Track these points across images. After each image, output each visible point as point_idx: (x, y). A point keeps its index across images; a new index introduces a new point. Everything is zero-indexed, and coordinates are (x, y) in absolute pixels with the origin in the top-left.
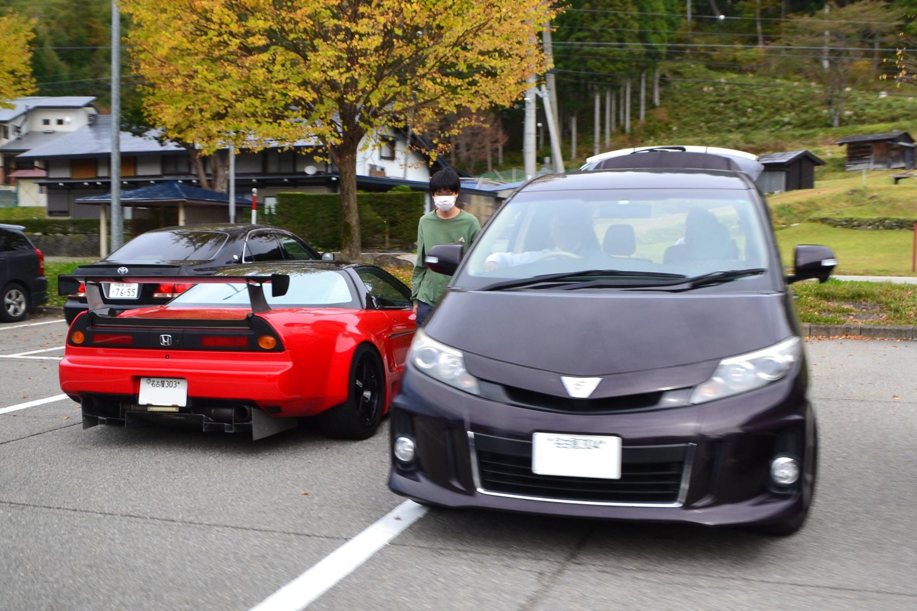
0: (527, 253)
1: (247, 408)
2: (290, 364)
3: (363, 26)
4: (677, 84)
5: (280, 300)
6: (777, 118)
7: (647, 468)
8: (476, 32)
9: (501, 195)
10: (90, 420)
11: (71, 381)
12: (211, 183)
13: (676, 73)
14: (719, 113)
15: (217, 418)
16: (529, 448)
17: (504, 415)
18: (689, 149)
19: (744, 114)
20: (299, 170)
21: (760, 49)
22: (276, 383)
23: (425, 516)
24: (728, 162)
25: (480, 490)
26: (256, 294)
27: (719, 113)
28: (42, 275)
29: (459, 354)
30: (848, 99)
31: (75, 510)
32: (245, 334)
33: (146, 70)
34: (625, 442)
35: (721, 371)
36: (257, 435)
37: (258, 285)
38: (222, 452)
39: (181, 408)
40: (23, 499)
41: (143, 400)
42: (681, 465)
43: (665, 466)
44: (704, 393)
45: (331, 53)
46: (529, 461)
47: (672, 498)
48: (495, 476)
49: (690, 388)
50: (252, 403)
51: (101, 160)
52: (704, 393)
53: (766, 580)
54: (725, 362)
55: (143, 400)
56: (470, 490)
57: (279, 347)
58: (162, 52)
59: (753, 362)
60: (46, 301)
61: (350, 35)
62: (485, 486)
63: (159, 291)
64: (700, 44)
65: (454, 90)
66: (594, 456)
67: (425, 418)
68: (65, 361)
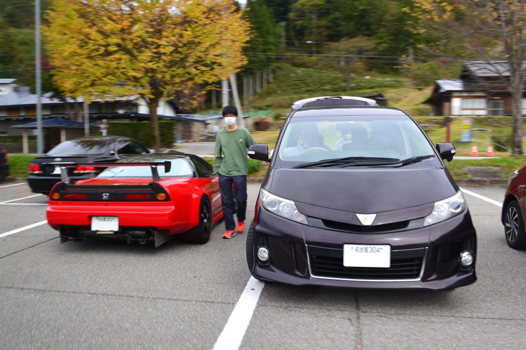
0: (289, 148)
1: (152, 231)
2: (173, 208)
3: (163, 42)
4: (279, 73)
5: (168, 174)
6: (323, 88)
7: (403, 262)
8: (213, 46)
9: (208, 122)
10: (64, 238)
11: (54, 221)
12: (76, 118)
13: (279, 68)
14: (298, 85)
15: (134, 236)
16: (341, 253)
17: (332, 236)
18: (344, 97)
19: (308, 86)
20: (116, 112)
21: (314, 58)
22: (167, 217)
23: (265, 286)
24: (366, 103)
25: (312, 276)
26: (154, 171)
27: (298, 85)
28: (6, 163)
29: (292, 203)
30: (353, 79)
31: (74, 292)
32: (151, 191)
33: (57, 63)
34: (393, 248)
35: (436, 209)
36: (157, 245)
37: (155, 167)
38: (428, 305)
39: (115, 232)
40: (41, 286)
41: (94, 228)
42: (421, 260)
43: (412, 260)
44: (429, 221)
45: (150, 54)
46: (341, 260)
47: (417, 276)
48: (318, 268)
49: (423, 218)
50: (154, 228)
51: (32, 108)
52: (429, 221)
53: (50, 242)
54: (436, 204)
55: (94, 228)
56: (308, 277)
57: (168, 199)
58: (66, 54)
59: (448, 203)
60: (8, 175)
61: (159, 46)
62: (314, 274)
63: (77, 170)
64: (289, 54)
65: (202, 72)
66: (379, 257)
67: (275, 237)
68: (49, 209)
